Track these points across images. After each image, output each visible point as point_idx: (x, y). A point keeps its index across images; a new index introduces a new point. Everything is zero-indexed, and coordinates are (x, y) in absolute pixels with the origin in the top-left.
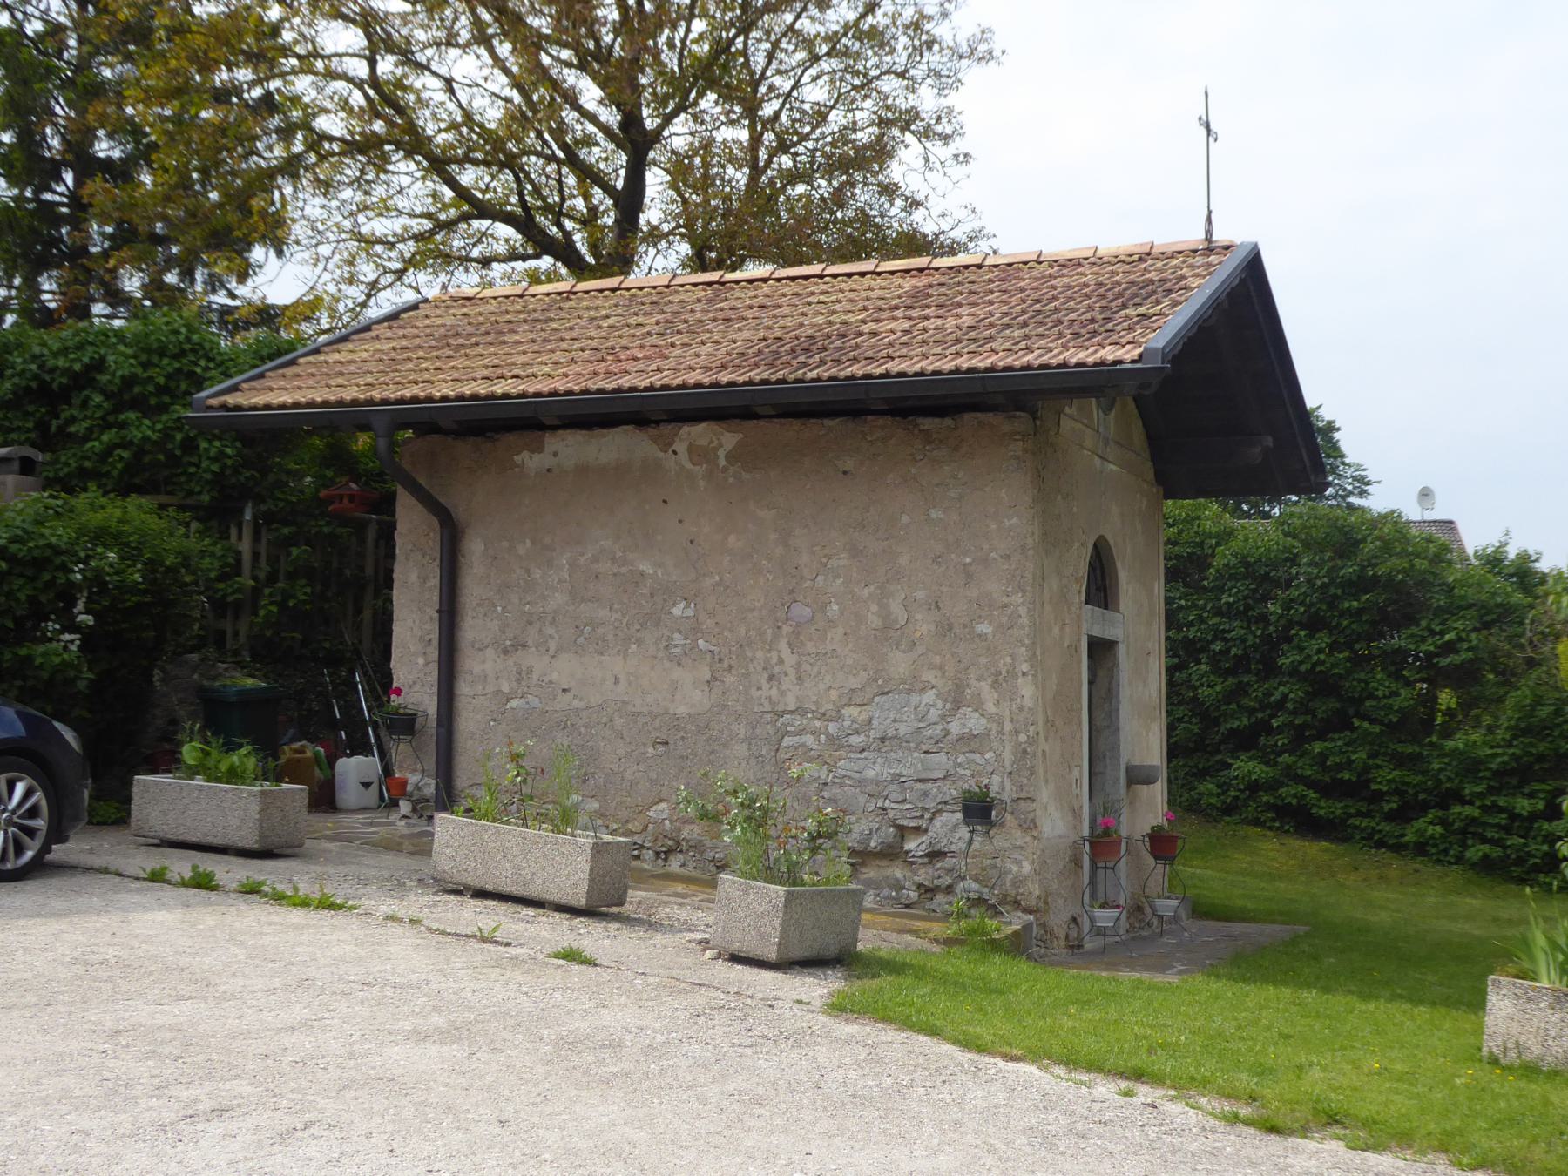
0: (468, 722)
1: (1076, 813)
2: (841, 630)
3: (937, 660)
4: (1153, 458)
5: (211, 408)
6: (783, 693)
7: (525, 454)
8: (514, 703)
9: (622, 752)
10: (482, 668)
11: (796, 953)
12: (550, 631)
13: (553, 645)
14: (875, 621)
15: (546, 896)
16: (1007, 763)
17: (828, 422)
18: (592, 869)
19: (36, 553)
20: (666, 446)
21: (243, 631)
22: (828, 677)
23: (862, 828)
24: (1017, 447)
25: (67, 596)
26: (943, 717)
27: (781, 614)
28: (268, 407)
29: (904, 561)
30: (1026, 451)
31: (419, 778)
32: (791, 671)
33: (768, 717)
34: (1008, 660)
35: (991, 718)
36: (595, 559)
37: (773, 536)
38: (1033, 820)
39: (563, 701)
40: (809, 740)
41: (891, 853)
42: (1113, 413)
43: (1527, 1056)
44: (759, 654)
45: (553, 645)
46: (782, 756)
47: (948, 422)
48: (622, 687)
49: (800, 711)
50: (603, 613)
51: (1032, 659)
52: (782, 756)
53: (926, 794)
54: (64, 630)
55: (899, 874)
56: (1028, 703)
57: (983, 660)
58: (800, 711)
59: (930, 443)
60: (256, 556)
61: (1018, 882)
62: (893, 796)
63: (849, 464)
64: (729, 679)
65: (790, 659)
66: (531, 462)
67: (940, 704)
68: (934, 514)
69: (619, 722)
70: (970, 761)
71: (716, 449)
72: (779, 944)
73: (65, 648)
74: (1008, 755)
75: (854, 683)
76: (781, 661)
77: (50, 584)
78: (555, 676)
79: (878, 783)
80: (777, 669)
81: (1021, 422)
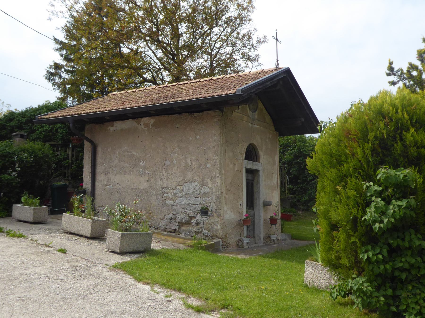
0: (98, 192)
1: (241, 213)
2: (176, 167)
3: (198, 174)
4: (274, 126)
5: (39, 119)
6: (164, 183)
7: (110, 127)
8: (107, 187)
9: (129, 198)
10: (101, 178)
11: (127, 250)
12: (114, 169)
13: (115, 173)
14: (184, 164)
15: (83, 234)
16: (214, 200)
17: (174, 115)
18: (92, 227)
19: (4, 154)
20: (139, 123)
21: (69, 172)
22: (173, 179)
23: (180, 217)
24: (216, 119)
25: (14, 163)
26: (199, 188)
27: (163, 164)
28: (50, 118)
29: (190, 149)
30: (218, 120)
31: (87, 205)
32: (165, 178)
33: (160, 189)
34: (214, 173)
35: (210, 188)
36: (124, 152)
37: (162, 144)
38: (220, 215)
39: (117, 186)
40: (169, 195)
41: (188, 223)
42: (257, 112)
43: (315, 285)
44: (159, 174)
45: (115, 173)
46: (164, 199)
47: (201, 113)
48: (129, 183)
49: (167, 187)
50: (126, 165)
51: (220, 173)
52: (164, 199)
53: (195, 208)
54: (13, 171)
55: (190, 228)
56: (219, 184)
57: (208, 174)
58: (167, 187)
59: (196, 119)
60: (73, 155)
61: (216, 231)
62: (188, 209)
63: (178, 126)
64: (152, 180)
65: (165, 175)
66: (111, 129)
67: (199, 185)
68: (198, 137)
69: (129, 191)
70: (205, 199)
71: (149, 124)
72: (120, 248)
73: (14, 176)
74: (214, 198)
75: (179, 180)
76: (163, 175)
77: (8, 161)
78: (115, 180)
79: (184, 205)
80: (162, 177)
81: (218, 112)
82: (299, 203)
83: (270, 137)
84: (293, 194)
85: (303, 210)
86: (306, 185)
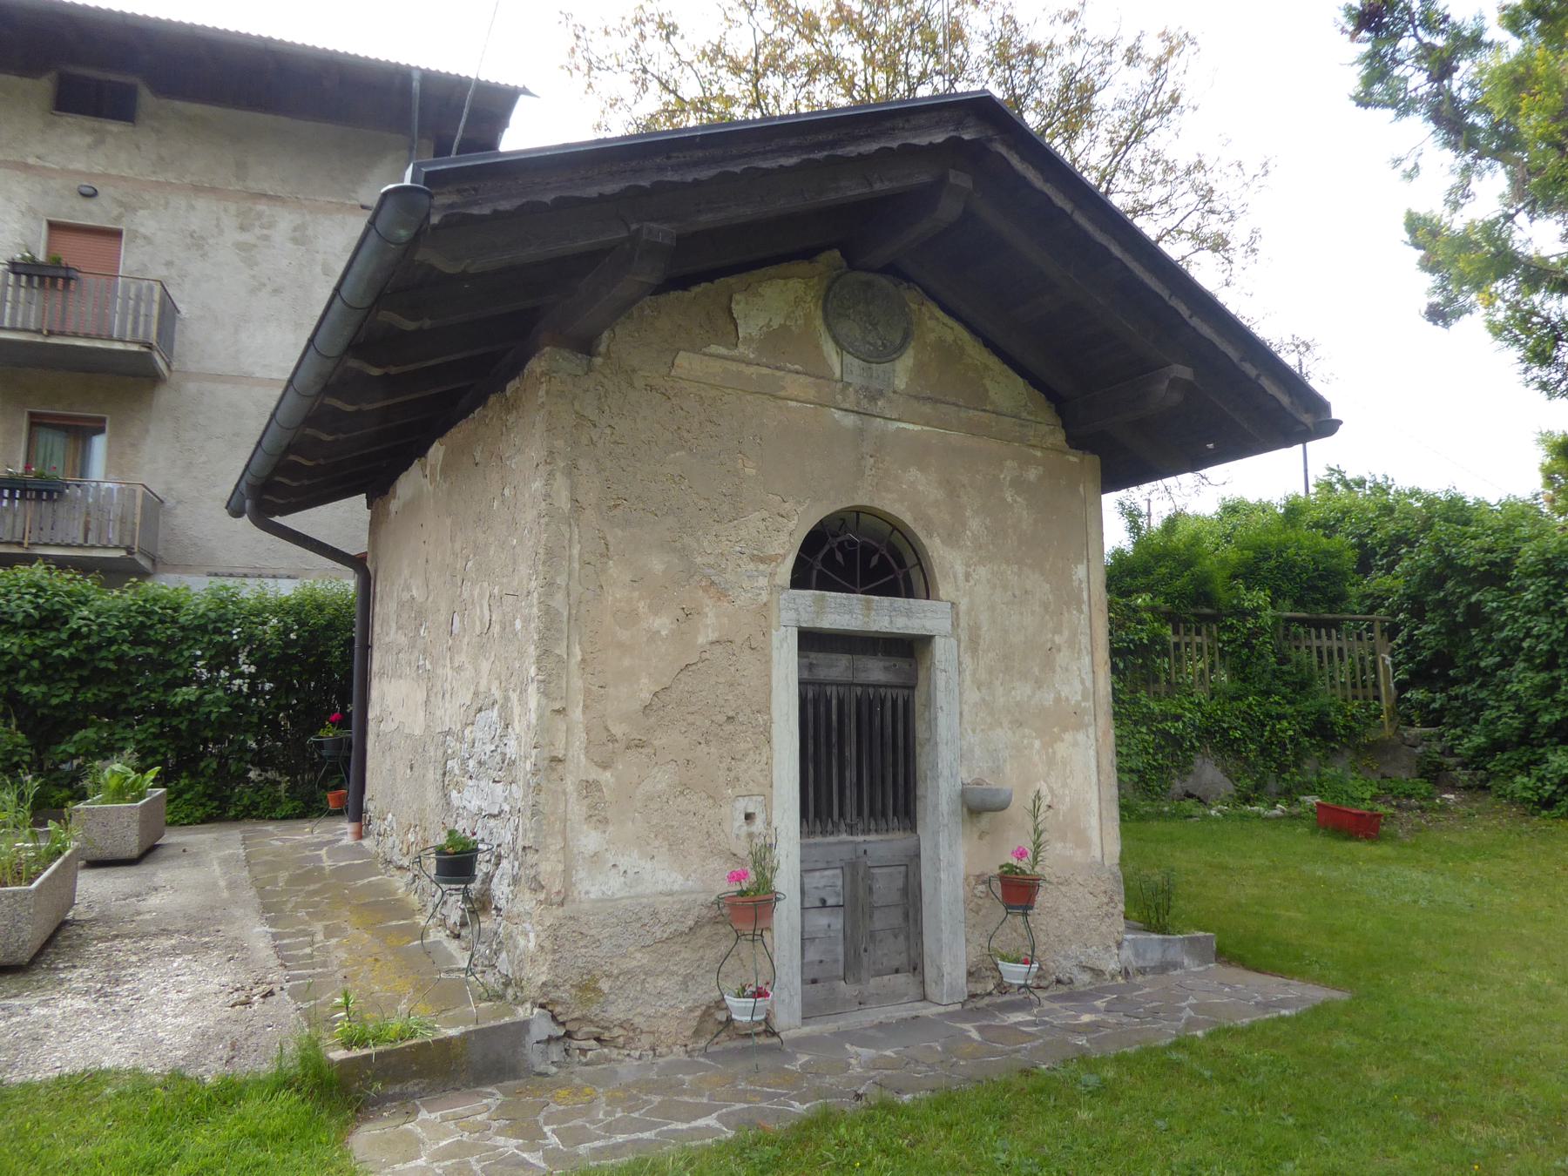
82: (1452, 761)
83: (1032, 474)
84: (1436, 723)
85: (1467, 788)
86: (1481, 686)
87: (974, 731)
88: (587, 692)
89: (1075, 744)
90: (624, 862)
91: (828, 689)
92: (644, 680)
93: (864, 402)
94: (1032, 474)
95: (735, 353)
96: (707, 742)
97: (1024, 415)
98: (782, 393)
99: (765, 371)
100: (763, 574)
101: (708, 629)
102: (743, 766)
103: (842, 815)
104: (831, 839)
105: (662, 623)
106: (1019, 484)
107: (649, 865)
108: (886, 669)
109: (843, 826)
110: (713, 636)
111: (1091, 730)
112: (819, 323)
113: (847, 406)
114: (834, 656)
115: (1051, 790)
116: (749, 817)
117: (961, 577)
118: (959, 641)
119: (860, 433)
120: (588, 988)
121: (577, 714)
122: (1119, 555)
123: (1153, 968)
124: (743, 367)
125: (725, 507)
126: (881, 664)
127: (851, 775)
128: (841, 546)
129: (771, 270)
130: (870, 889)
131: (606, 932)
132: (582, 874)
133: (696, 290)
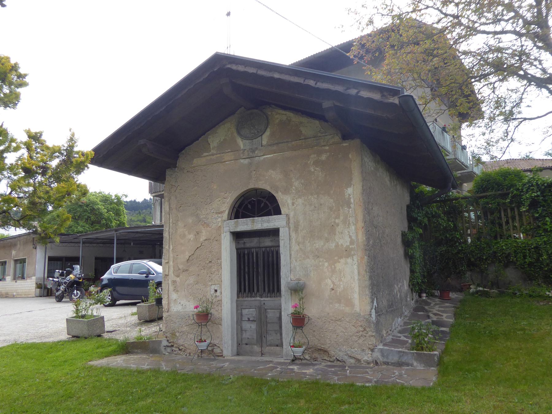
87: (296, 261)
88: (174, 257)
89: (346, 263)
90: (182, 302)
91: (252, 250)
92: (187, 253)
93: (251, 154)
94: (324, 157)
95: (211, 153)
96: (204, 269)
97: (319, 135)
98: (223, 161)
99: (218, 155)
100: (219, 217)
101: (203, 236)
102: (214, 276)
103: (258, 291)
104: (253, 299)
105: (191, 237)
106: (317, 163)
107: (188, 303)
108: (271, 241)
109: (258, 295)
110: (204, 238)
111: (355, 257)
112: (235, 134)
113: (244, 157)
114: (253, 239)
115: (333, 283)
116: (216, 291)
117: (290, 204)
118: (289, 228)
119: (250, 164)
120: (173, 334)
121: (171, 263)
122: (349, 185)
123: (392, 363)
124: (212, 157)
125: (208, 200)
126: (270, 239)
127: (261, 278)
128: (250, 203)
129: (221, 123)
130: (267, 317)
131: (177, 321)
132: (172, 305)
133: (200, 139)
